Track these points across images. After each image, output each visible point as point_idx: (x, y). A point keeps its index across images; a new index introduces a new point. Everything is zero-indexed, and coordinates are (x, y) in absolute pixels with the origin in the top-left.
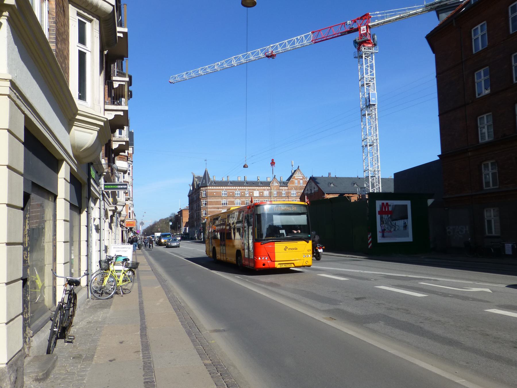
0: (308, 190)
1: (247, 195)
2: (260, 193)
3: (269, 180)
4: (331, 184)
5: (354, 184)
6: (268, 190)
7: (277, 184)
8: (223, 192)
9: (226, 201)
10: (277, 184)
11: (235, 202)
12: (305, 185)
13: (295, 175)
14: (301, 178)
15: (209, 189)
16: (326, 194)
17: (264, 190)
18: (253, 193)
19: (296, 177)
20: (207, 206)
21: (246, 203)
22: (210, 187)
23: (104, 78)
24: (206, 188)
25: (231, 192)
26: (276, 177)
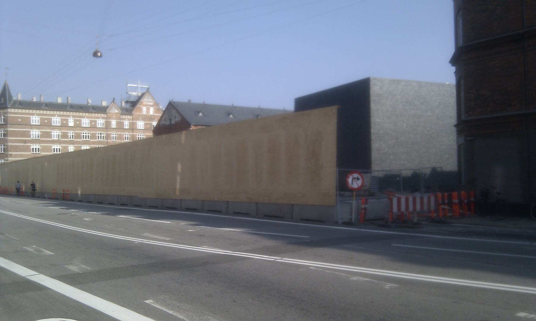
0: (165, 120)
1: (126, 127)
2: (91, 122)
3: (104, 104)
4: (199, 112)
5: (229, 114)
6: (103, 118)
7: (116, 111)
8: (33, 117)
9: (88, 133)
10: (116, 111)
11: (112, 136)
12: (161, 115)
13: (143, 100)
14: (152, 104)
15: (11, 113)
16: (194, 125)
17: (98, 118)
18: (95, 122)
19: (144, 103)
20: (6, 138)
21: (126, 137)
22: (13, 110)
23: (453, 12)
24: (5, 111)
25: (46, 118)
26: (116, 101)
